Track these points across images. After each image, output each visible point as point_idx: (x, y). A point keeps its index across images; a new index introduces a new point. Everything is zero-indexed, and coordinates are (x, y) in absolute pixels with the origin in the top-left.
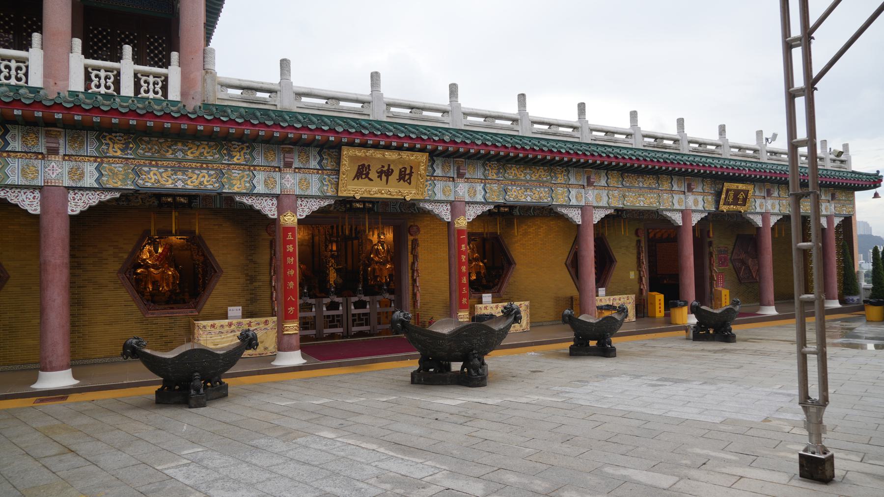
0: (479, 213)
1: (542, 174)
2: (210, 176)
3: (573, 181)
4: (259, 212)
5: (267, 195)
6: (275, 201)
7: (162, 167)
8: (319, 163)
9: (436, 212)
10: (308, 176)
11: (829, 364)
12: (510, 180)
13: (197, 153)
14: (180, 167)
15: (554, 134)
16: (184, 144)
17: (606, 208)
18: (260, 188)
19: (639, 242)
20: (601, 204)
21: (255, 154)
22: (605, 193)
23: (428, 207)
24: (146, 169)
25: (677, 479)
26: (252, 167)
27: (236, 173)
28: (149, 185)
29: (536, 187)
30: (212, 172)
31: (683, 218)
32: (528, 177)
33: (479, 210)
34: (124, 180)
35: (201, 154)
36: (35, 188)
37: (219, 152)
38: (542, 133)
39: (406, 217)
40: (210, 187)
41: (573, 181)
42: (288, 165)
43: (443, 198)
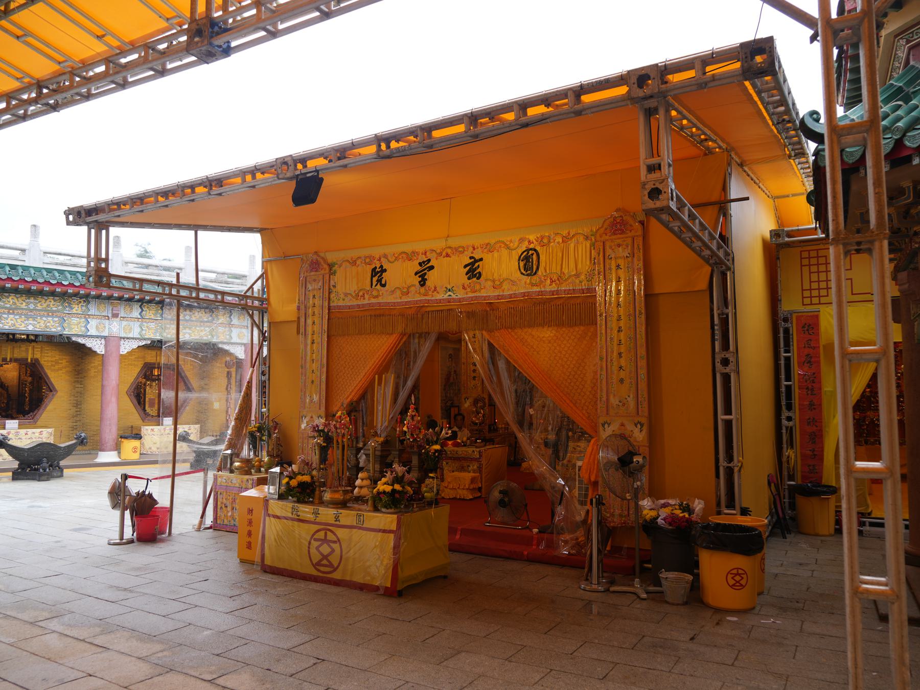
0: (135, 346)
1: (53, 304)
2: (54, 321)
3: (235, 321)
4: (90, 349)
5: (97, 337)
6: (103, 341)
7: (18, 314)
8: (140, 314)
9: (89, 345)
10: (132, 324)
11: (373, 533)
12: (6, 308)
13: (45, 305)
14: (29, 315)
15: (74, 266)
16: (35, 299)
17: (140, 339)
18: (93, 332)
19: (229, 373)
20: (131, 335)
21: (90, 306)
22: (137, 324)
23: (226, 347)
24: (5, 316)
25: (217, 682)
26: (87, 317)
27: (75, 320)
28: (7, 327)
29: (41, 317)
30: (56, 319)
31: (106, 346)
32: (32, 306)
33: (135, 345)
34: (154, 333)
35: (48, 306)
36: (102, 337)
37: (62, 305)
38: (211, 281)
39: (77, 352)
40: (54, 330)
41: (235, 321)
42: (115, 316)
43: (239, 341)
